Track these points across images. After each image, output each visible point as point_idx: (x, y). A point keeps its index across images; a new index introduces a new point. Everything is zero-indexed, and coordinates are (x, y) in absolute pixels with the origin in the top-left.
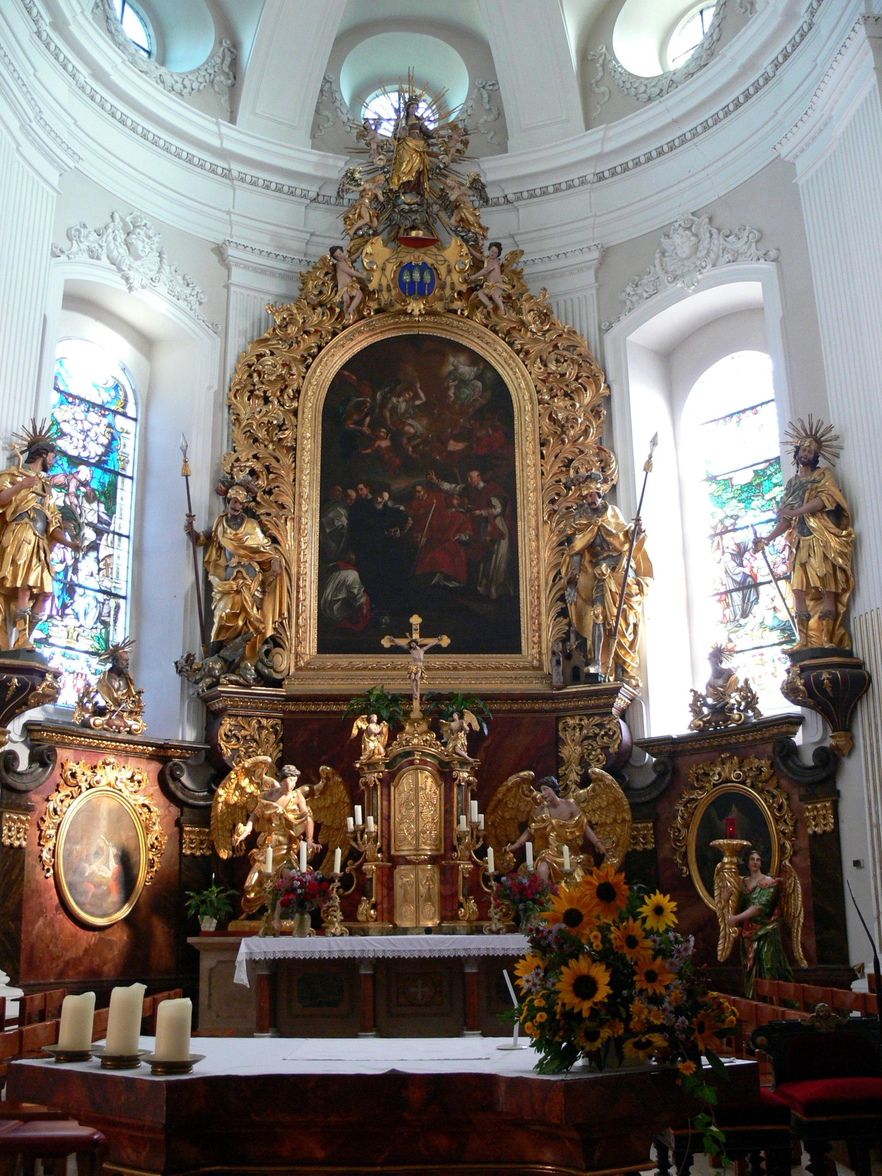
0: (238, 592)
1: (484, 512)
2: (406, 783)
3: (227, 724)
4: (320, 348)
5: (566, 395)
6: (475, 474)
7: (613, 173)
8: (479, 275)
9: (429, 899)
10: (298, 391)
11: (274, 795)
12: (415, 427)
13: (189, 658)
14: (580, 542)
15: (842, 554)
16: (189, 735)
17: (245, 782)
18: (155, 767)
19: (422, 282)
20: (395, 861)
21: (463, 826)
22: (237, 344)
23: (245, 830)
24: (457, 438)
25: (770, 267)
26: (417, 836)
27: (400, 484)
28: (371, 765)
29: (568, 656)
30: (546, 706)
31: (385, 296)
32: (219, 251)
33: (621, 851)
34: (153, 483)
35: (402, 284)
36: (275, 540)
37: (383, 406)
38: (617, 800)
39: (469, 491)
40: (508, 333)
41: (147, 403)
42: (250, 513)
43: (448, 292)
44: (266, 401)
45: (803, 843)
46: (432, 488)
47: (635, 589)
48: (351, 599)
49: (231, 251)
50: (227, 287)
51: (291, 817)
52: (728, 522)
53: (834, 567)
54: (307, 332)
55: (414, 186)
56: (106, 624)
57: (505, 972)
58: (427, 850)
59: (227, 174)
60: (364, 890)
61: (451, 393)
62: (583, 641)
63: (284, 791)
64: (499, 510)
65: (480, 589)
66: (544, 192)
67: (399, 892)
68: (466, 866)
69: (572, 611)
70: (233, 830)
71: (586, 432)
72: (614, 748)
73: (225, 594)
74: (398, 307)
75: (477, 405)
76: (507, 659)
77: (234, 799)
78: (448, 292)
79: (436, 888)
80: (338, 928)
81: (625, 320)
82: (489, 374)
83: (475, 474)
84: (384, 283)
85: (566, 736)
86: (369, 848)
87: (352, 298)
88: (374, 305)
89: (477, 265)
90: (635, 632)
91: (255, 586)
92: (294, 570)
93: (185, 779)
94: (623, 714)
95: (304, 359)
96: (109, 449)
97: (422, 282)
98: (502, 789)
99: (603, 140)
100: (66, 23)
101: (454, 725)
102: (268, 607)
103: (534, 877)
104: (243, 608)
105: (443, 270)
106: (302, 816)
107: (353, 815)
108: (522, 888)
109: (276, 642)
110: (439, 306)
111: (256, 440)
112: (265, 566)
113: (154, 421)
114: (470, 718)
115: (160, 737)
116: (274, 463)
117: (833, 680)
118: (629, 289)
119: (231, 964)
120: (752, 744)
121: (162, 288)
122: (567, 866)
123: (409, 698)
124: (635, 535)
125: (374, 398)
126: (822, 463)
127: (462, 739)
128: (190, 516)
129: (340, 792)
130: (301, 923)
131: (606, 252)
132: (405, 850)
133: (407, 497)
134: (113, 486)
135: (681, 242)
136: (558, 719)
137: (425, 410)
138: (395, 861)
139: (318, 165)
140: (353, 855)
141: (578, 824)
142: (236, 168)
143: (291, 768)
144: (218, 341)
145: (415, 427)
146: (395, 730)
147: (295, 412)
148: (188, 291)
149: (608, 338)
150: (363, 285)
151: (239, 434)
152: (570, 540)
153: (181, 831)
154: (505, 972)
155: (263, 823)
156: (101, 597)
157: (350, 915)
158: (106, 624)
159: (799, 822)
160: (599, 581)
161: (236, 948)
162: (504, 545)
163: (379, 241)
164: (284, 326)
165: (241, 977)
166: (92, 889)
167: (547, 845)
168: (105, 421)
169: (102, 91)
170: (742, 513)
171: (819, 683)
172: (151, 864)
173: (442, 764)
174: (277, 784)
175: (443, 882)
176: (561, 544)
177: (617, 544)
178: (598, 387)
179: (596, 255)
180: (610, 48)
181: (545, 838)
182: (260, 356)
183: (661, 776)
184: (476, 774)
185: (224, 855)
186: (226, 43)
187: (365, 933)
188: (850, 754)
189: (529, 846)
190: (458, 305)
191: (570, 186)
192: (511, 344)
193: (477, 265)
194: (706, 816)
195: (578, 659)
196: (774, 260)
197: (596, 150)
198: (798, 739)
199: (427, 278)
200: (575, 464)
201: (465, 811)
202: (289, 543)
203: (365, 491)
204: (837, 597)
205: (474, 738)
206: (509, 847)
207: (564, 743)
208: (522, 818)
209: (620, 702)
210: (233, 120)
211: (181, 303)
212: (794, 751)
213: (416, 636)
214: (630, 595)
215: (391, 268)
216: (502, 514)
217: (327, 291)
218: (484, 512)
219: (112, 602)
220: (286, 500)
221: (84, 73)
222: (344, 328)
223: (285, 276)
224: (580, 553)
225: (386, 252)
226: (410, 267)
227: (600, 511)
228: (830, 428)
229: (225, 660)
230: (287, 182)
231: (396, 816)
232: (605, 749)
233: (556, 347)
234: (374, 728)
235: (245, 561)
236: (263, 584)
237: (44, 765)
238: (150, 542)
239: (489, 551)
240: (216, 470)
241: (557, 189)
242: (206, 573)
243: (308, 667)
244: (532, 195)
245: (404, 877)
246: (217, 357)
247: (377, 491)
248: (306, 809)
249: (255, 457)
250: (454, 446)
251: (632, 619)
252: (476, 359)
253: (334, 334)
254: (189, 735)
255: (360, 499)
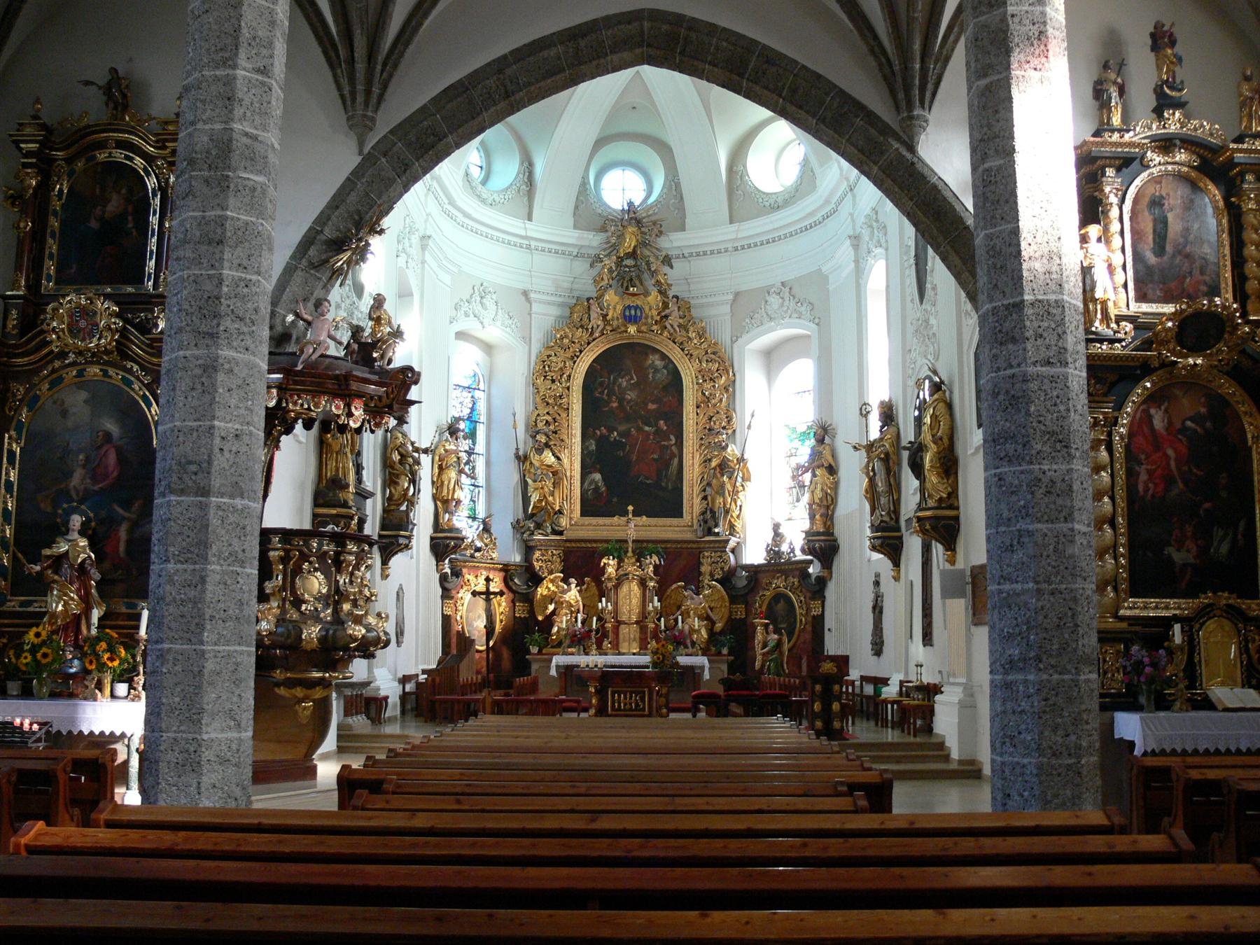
0: (542, 488)
1: (666, 443)
2: (624, 589)
3: (537, 554)
4: (581, 352)
5: (711, 379)
6: (662, 422)
7: (743, 248)
8: (667, 311)
9: (635, 640)
10: (570, 376)
11: (564, 592)
12: (631, 395)
13: (518, 521)
14: (714, 464)
15: (830, 488)
16: (517, 558)
17: (550, 585)
18: (502, 574)
19: (636, 316)
20: (619, 623)
21: (651, 608)
22: (536, 347)
23: (551, 607)
24: (653, 402)
25: (814, 326)
26: (629, 612)
27: (622, 428)
28: (609, 579)
29: (706, 522)
30: (694, 546)
31: (615, 323)
32: (525, 294)
33: (724, 620)
34: (494, 426)
35: (625, 317)
36: (558, 458)
37: (614, 383)
38: (722, 597)
39: (658, 432)
40: (682, 343)
41: (490, 382)
42: (547, 445)
43: (650, 320)
44: (553, 381)
45: (810, 619)
46: (639, 430)
47: (741, 488)
48: (597, 489)
49: (532, 295)
50: (530, 314)
51: (572, 602)
52: (793, 451)
53: (827, 494)
54: (574, 342)
55: (633, 255)
56: (474, 502)
57: (34, 160)
58: (634, 618)
59: (528, 247)
60: (605, 635)
61: (650, 376)
62: (712, 512)
63: (569, 590)
64: (674, 442)
65: (663, 484)
66: (705, 253)
67: (621, 637)
68: (652, 626)
69: (709, 498)
70: (546, 608)
71: (721, 400)
72: (726, 568)
73: (536, 489)
74: (623, 329)
75: (664, 383)
76: (675, 521)
77: (545, 593)
78: (650, 320)
79: (638, 636)
80: (594, 652)
81: (745, 337)
82: (671, 366)
83: (662, 422)
84: (615, 315)
85: (704, 561)
86: (608, 617)
87: (598, 326)
88: (609, 328)
89: (666, 306)
90: (740, 510)
91: (550, 485)
92: (568, 474)
93: (516, 580)
94: (733, 551)
95: (572, 358)
96: (472, 409)
97: (636, 316)
98: (669, 591)
99: (737, 231)
100: (455, 201)
101: (648, 561)
102: (556, 494)
103: (682, 632)
104: (545, 497)
105: (647, 309)
106: (577, 601)
107: (601, 601)
108: (675, 637)
109: (560, 512)
110: (644, 328)
111: (548, 404)
112: (555, 473)
113: (494, 391)
114: (655, 558)
115: (505, 560)
116: (558, 417)
117: (821, 548)
118: (747, 320)
119: (549, 668)
120: (792, 570)
121: (498, 323)
122: (696, 627)
123: (626, 541)
124: (741, 460)
125: (609, 379)
126: (827, 440)
127: (651, 568)
128: (517, 449)
129: (594, 590)
130: (579, 650)
131: (737, 294)
132: (624, 618)
133: (626, 434)
134: (475, 429)
135: (774, 301)
136: (700, 552)
137: (633, 387)
138: (619, 623)
139: (579, 238)
140: (600, 619)
141: (703, 608)
142: (533, 244)
143: (573, 580)
144: (527, 348)
145: (631, 395)
146: (620, 561)
147: (568, 388)
148: (510, 322)
149: (735, 346)
150: (605, 316)
151: (538, 400)
152: (710, 460)
153: (514, 606)
154: (34, 160)
155: (559, 604)
156: (472, 488)
157: (599, 646)
158: (474, 502)
159: (809, 610)
160: (722, 486)
161: (551, 661)
162: (676, 461)
163: (611, 292)
164: (562, 338)
165: (553, 672)
166: (477, 633)
167: (689, 617)
168: (470, 395)
169: (467, 221)
170: (800, 447)
171: (814, 549)
172: (501, 621)
173: (642, 579)
174: (566, 587)
175: (641, 633)
176: (705, 461)
177: (732, 465)
178: (728, 374)
179: (731, 297)
180: (745, 166)
181: (688, 613)
182: (549, 356)
183: (749, 582)
184: (657, 583)
185: (540, 618)
186: (526, 164)
187: (606, 654)
188: (830, 579)
189: (680, 617)
190: (655, 328)
191: (719, 252)
192: (683, 350)
193: (666, 306)
194: (770, 604)
195: (711, 523)
196: (817, 324)
197: (734, 236)
198: (811, 570)
199: (639, 313)
200: (714, 419)
201: (652, 601)
202: (565, 461)
203: (604, 431)
204: (828, 507)
205: (656, 567)
206: (671, 617)
207: (703, 564)
208: (679, 603)
209: (732, 544)
210: (530, 218)
211: (508, 329)
212: (809, 575)
213: (630, 516)
214: (738, 492)
215: (620, 308)
216: (675, 444)
217: (585, 319)
218: (666, 443)
219: (477, 490)
220: (565, 437)
221: (460, 217)
222: (594, 340)
223: (561, 305)
224: (715, 469)
225: (617, 299)
226: (629, 307)
227: (725, 448)
228: (831, 425)
229: (536, 522)
230: (560, 248)
231: (620, 603)
232: (722, 569)
233: (707, 353)
234: (611, 562)
235: (545, 472)
236: (554, 483)
237: (457, 577)
238: (494, 459)
239: (667, 464)
240: (528, 419)
241: (712, 253)
242: (524, 476)
243: (576, 524)
244: (698, 255)
245: (624, 630)
246: (526, 356)
247: (611, 430)
248: (579, 598)
249: (548, 413)
250: (651, 406)
251: (739, 503)
252: (664, 357)
253: (589, 344)
254: (517, 558)
255: (602, 436)
